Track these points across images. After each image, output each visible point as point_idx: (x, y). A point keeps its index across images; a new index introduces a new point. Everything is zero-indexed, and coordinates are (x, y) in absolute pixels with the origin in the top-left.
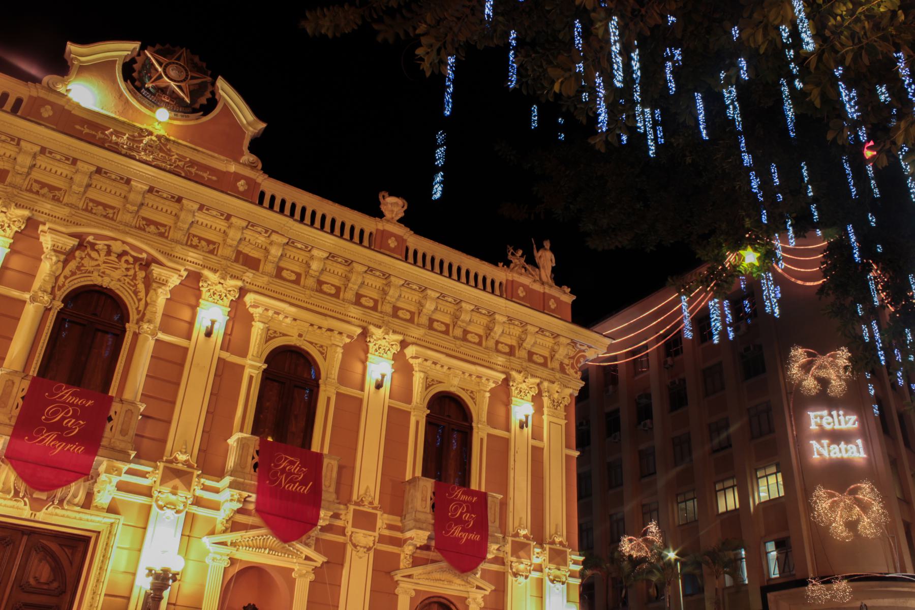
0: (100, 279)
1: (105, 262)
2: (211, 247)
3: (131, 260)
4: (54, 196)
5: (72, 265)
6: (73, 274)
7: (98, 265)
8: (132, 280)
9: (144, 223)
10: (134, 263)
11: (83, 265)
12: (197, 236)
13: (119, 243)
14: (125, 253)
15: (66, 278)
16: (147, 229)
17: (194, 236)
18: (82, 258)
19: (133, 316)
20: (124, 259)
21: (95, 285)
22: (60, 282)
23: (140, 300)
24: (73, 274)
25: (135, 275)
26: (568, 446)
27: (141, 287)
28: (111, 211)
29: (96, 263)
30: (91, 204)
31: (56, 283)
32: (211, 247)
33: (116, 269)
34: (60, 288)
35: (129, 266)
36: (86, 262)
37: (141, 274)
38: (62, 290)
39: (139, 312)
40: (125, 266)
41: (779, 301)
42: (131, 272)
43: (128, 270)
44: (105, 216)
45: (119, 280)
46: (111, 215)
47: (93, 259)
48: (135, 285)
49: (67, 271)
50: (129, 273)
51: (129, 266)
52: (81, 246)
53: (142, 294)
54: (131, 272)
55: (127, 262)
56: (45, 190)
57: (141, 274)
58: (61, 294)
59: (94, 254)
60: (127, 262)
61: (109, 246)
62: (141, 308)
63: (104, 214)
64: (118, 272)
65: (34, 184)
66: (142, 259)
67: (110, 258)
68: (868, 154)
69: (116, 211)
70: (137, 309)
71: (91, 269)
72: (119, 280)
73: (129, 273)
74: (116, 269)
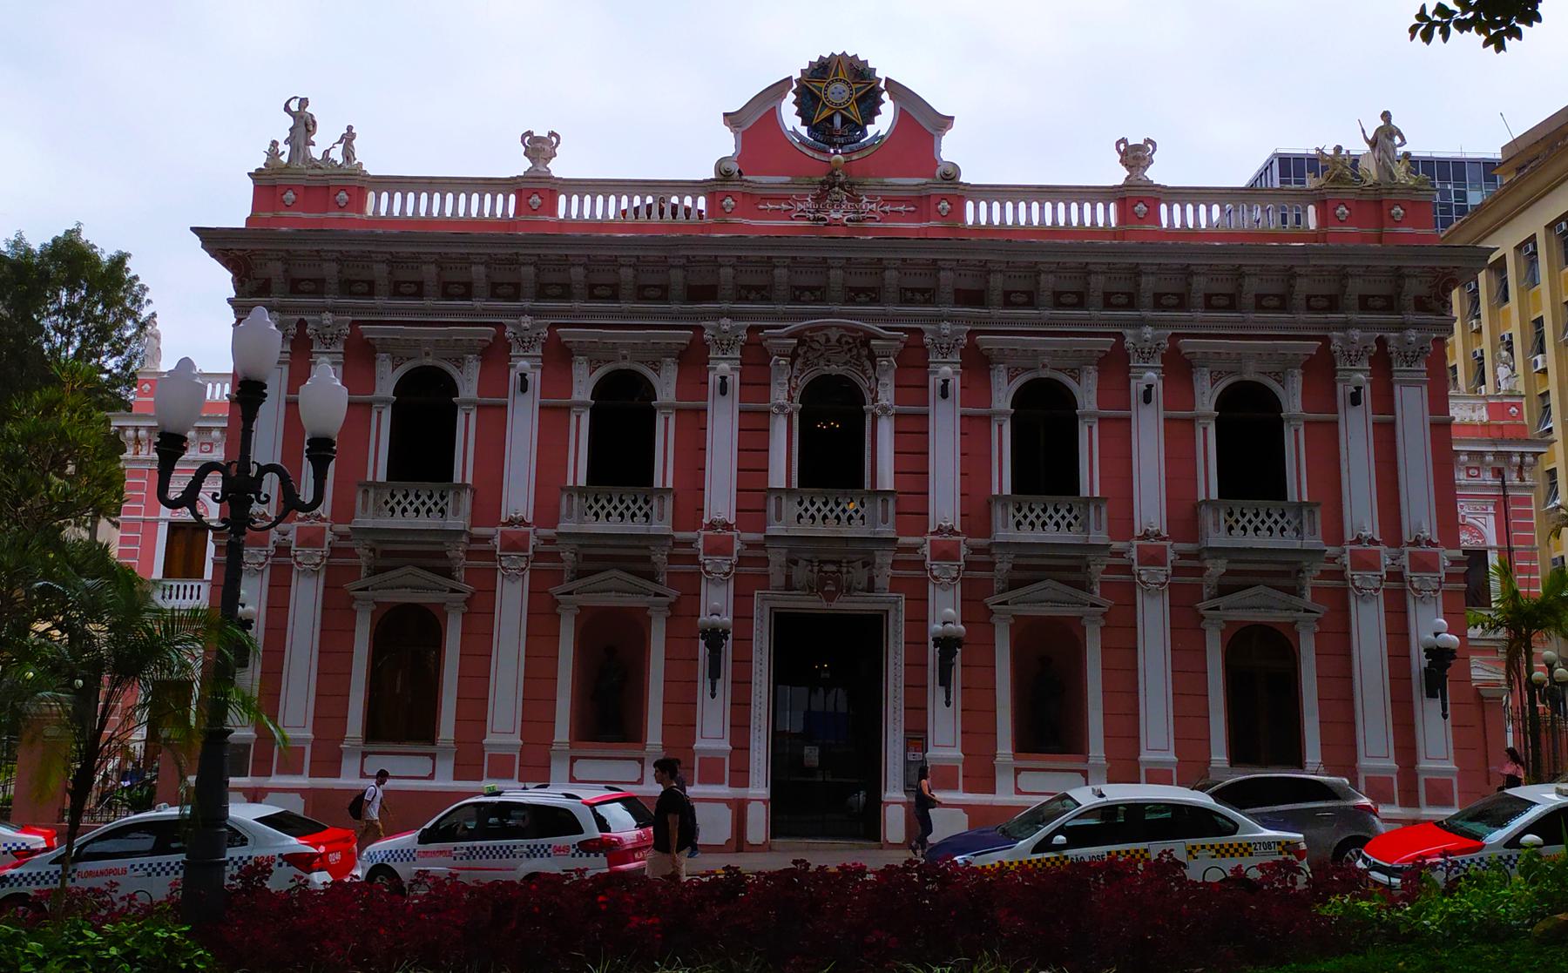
5: (799, 362)
6: (802, 371)
19: (868, 397)
27: (867, 364)
42: (855, 352)
52: (801, 343)
53: (870, 372)
57: (865, 352)
58: (797, 395)
60: (847, 343)
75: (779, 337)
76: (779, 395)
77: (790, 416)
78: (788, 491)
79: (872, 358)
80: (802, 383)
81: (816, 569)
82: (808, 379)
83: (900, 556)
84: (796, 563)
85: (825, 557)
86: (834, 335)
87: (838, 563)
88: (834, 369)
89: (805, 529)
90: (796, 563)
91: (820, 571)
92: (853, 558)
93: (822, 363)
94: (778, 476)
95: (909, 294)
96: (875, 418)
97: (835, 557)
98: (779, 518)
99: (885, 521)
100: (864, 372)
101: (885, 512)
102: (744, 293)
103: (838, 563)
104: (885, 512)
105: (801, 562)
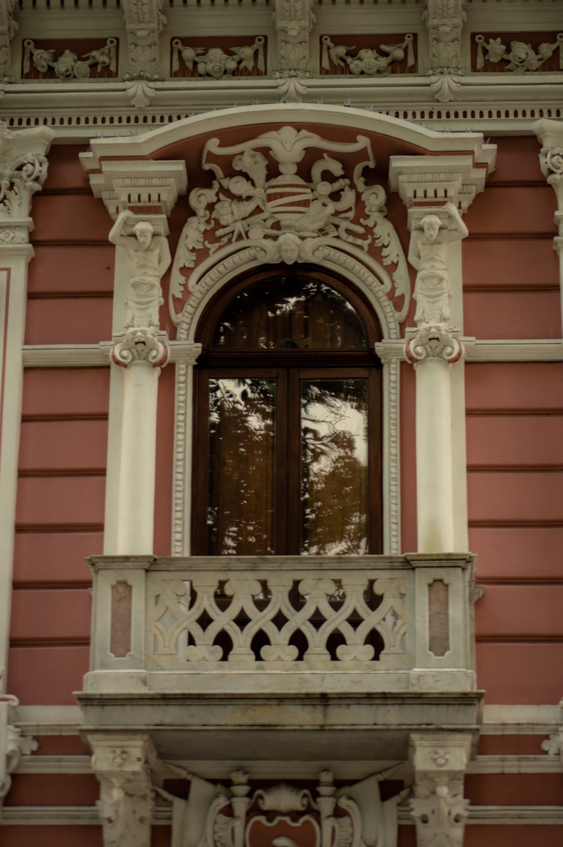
0: (268, 244)
1: (270, 198)
2: (546, 50)
3: (336, 168)
4: (93, 66)
5: (193, 233)
6: (201, 254)
7: (258, 210)
8: (355, 221)
9: (341, 50)
10: (348, 174)
11: (219, 225)
12: (494, 35)
13: (288, 133)
14: (312, 155)
15: (186, 271)
16: (354, 65)
17: (489, 36)
18: (211, 207)
19: (389, 318)
20: (316, 171)
21: (265, 268)
22: (176, 290)
23: (392, 268)
24: (201, 254)
25: (359, 202)
26: (258, 422)
27: (385, 231)
28: (247, 52)
29: (250, 207)
30: (189, 53)
31: (165, 295)
32: (546, 50)
33: (306, 204)
34: (180, 303)
35: (337, 186)
36: (228, 212)
37: (375, 197)
38: (188, 308)
39: (398, 306)
40: (325, 188)
41: (477, 339)
42: (348, 198)
43: (335, 196)
44: (236, 73)
45: (322, 232)
46: (250, 65)
47: (239, 198)
48: (369, 230)
49: (184, 257)
50: (342, 205)
51: (337, 186)
52: (199, 178)
53: (393, 252)
54: (348, 198)
55: (327, 176)
56: (67, 61)
57: (375, 197)
58: (187, 320)
59: (238, 186)
60: (327, 176)
61: (265, 151)
62: (402, 288)
63: (232, 65)
64: (315, 207)
65: (38, 53)
66: (362, 155)
67: (279, 180)
68: (239, 432)
69: (258, 45)
70: (391, 295)
71: (239, 227)
72: (322, 232)
73: (342, 205)
74: (306, 204)
75: (131, 162)
76: (134, 314)
77: (167, 372)
78: (152, 565)
79: (396, 210)
80: (201, 291)
81: (241, 806)
82: (217, 280)
83: (491, 764)
84: (181, 789)
85: (264, 769)
86: (288, 147)
87: (310, 786)
88: (296, 245)
89: (197, 669)
90: (181, 789)
91: (254, 810)
92: (350, 769)
93: (256, 234)
94: (131, 515)
95: (496, 48)
96: (408, 369)
97: (300, 770)
98: (121, 643)
99: (439, 645)
100: (376, 252)
101: (439, 618)
102: (42, 57)
103: (310, 786)
104: (439, 618)
105: (199, 789)
